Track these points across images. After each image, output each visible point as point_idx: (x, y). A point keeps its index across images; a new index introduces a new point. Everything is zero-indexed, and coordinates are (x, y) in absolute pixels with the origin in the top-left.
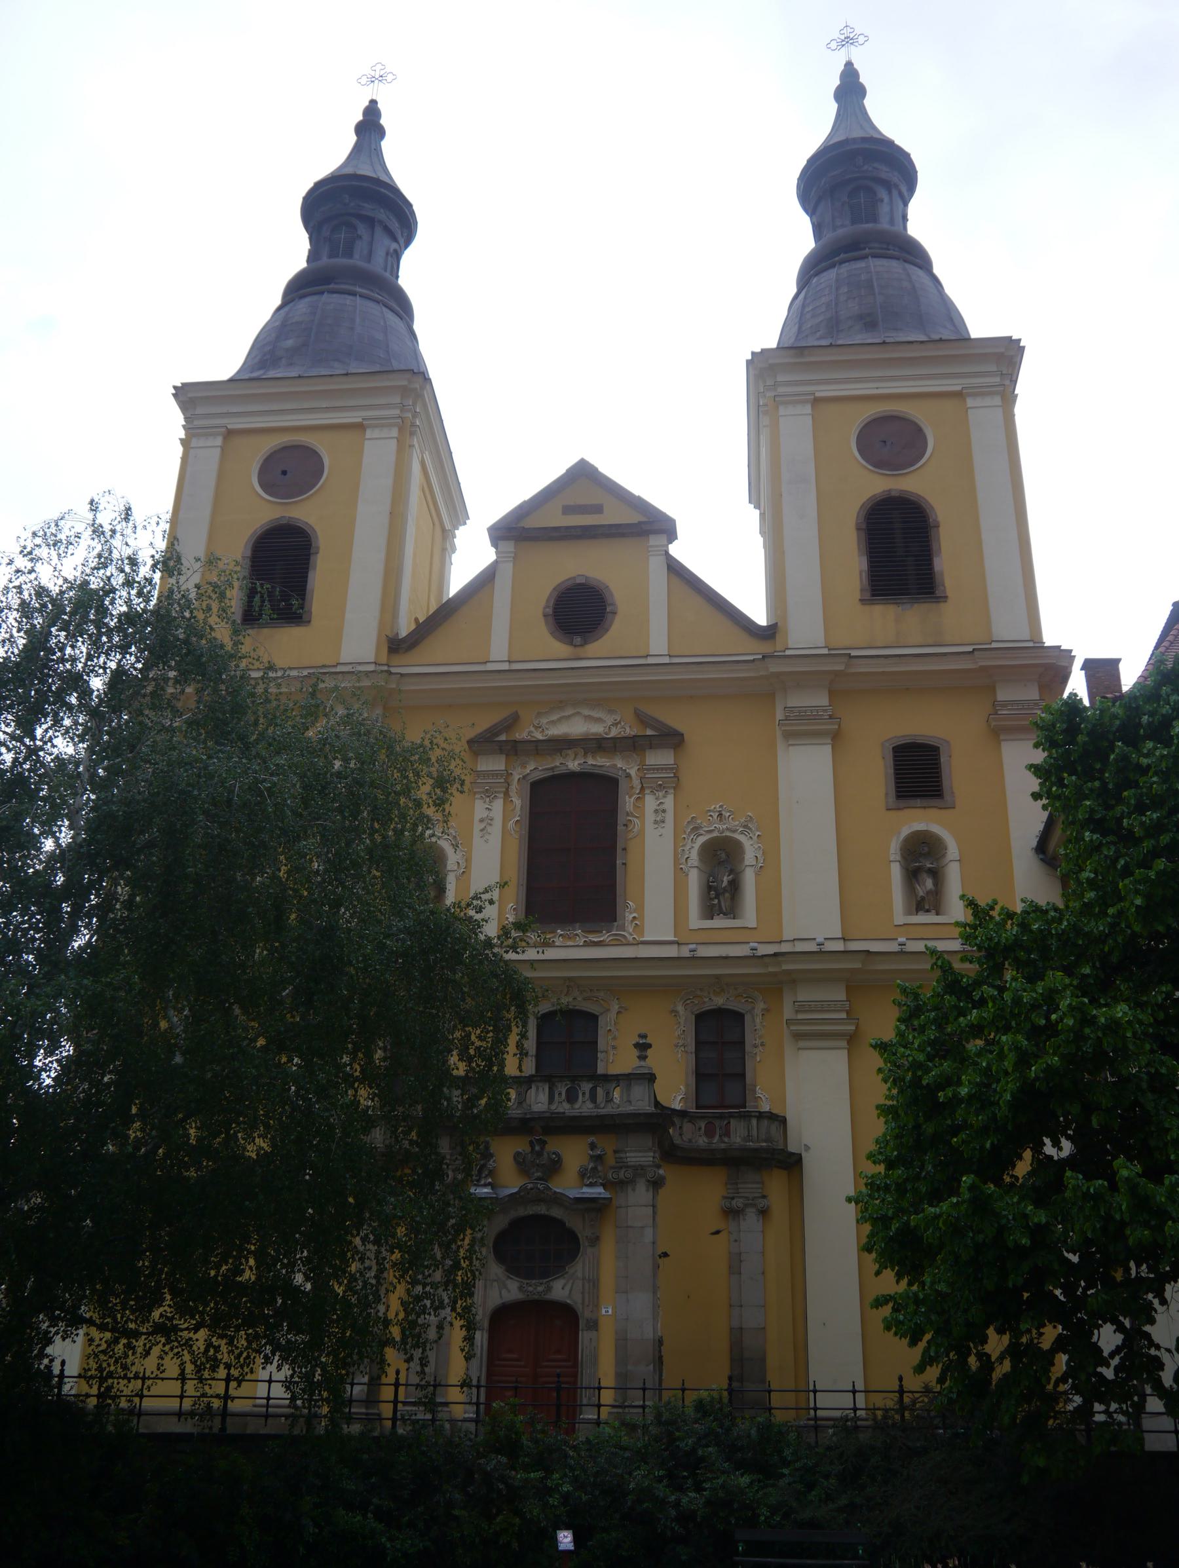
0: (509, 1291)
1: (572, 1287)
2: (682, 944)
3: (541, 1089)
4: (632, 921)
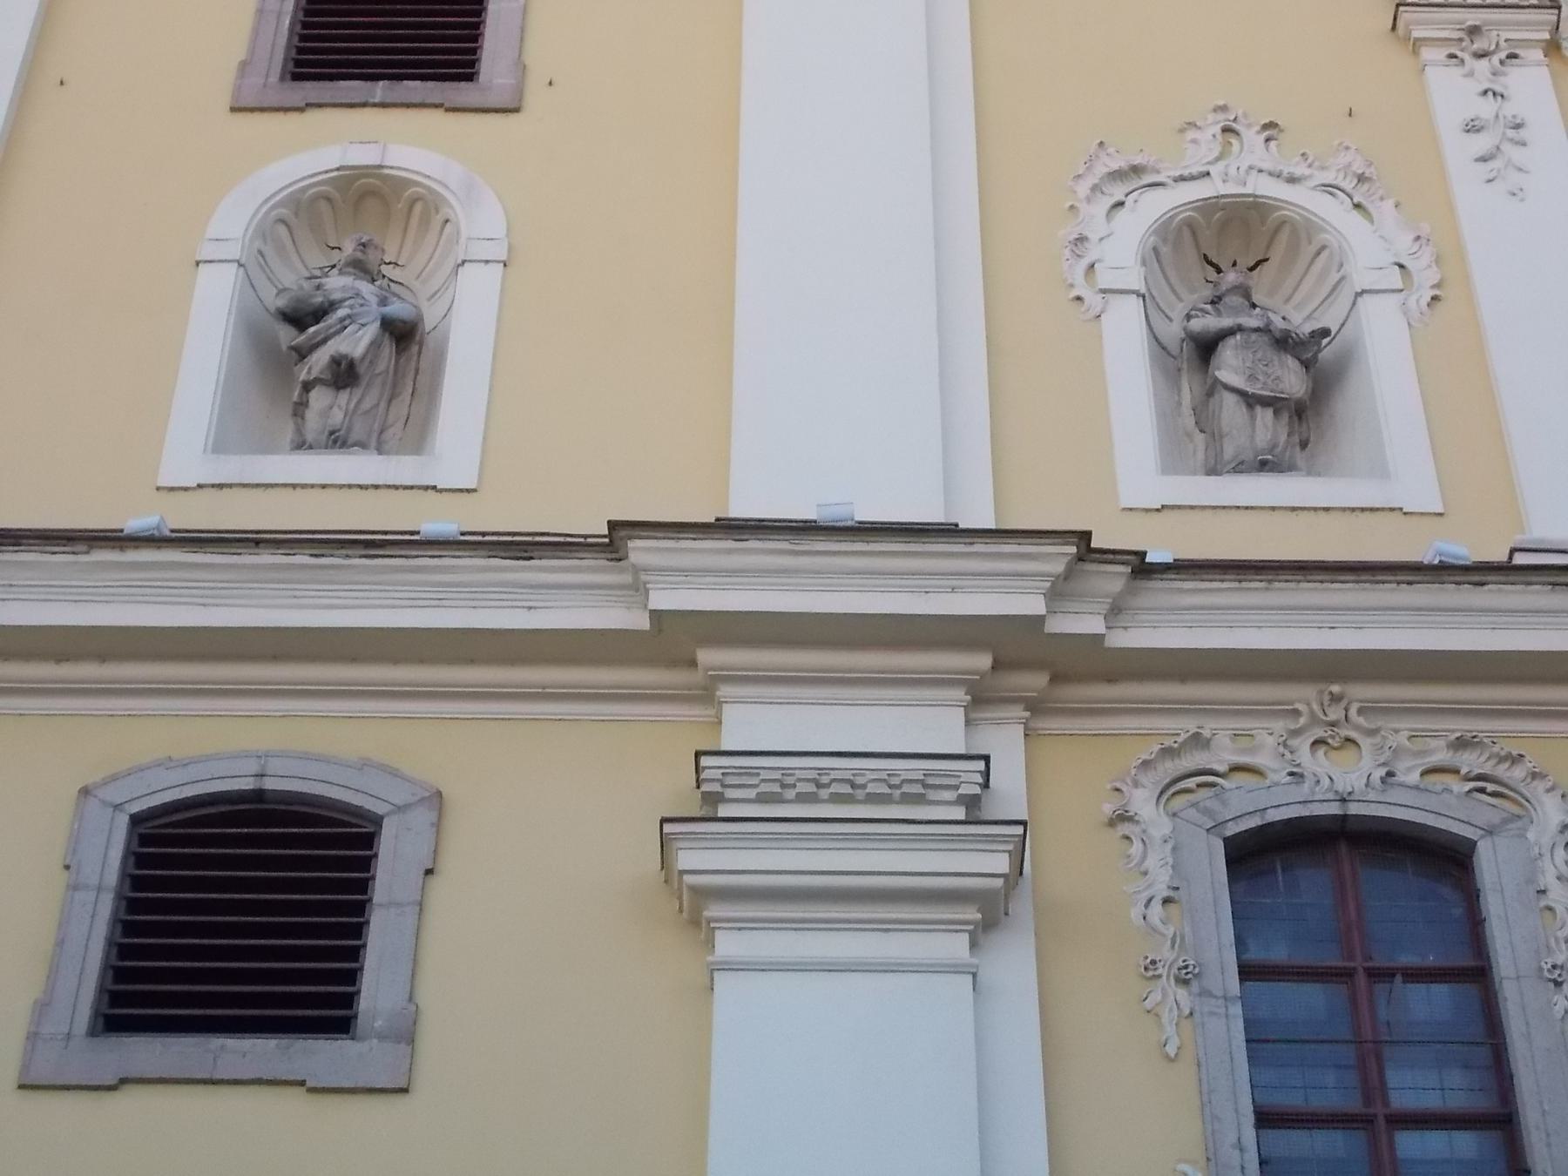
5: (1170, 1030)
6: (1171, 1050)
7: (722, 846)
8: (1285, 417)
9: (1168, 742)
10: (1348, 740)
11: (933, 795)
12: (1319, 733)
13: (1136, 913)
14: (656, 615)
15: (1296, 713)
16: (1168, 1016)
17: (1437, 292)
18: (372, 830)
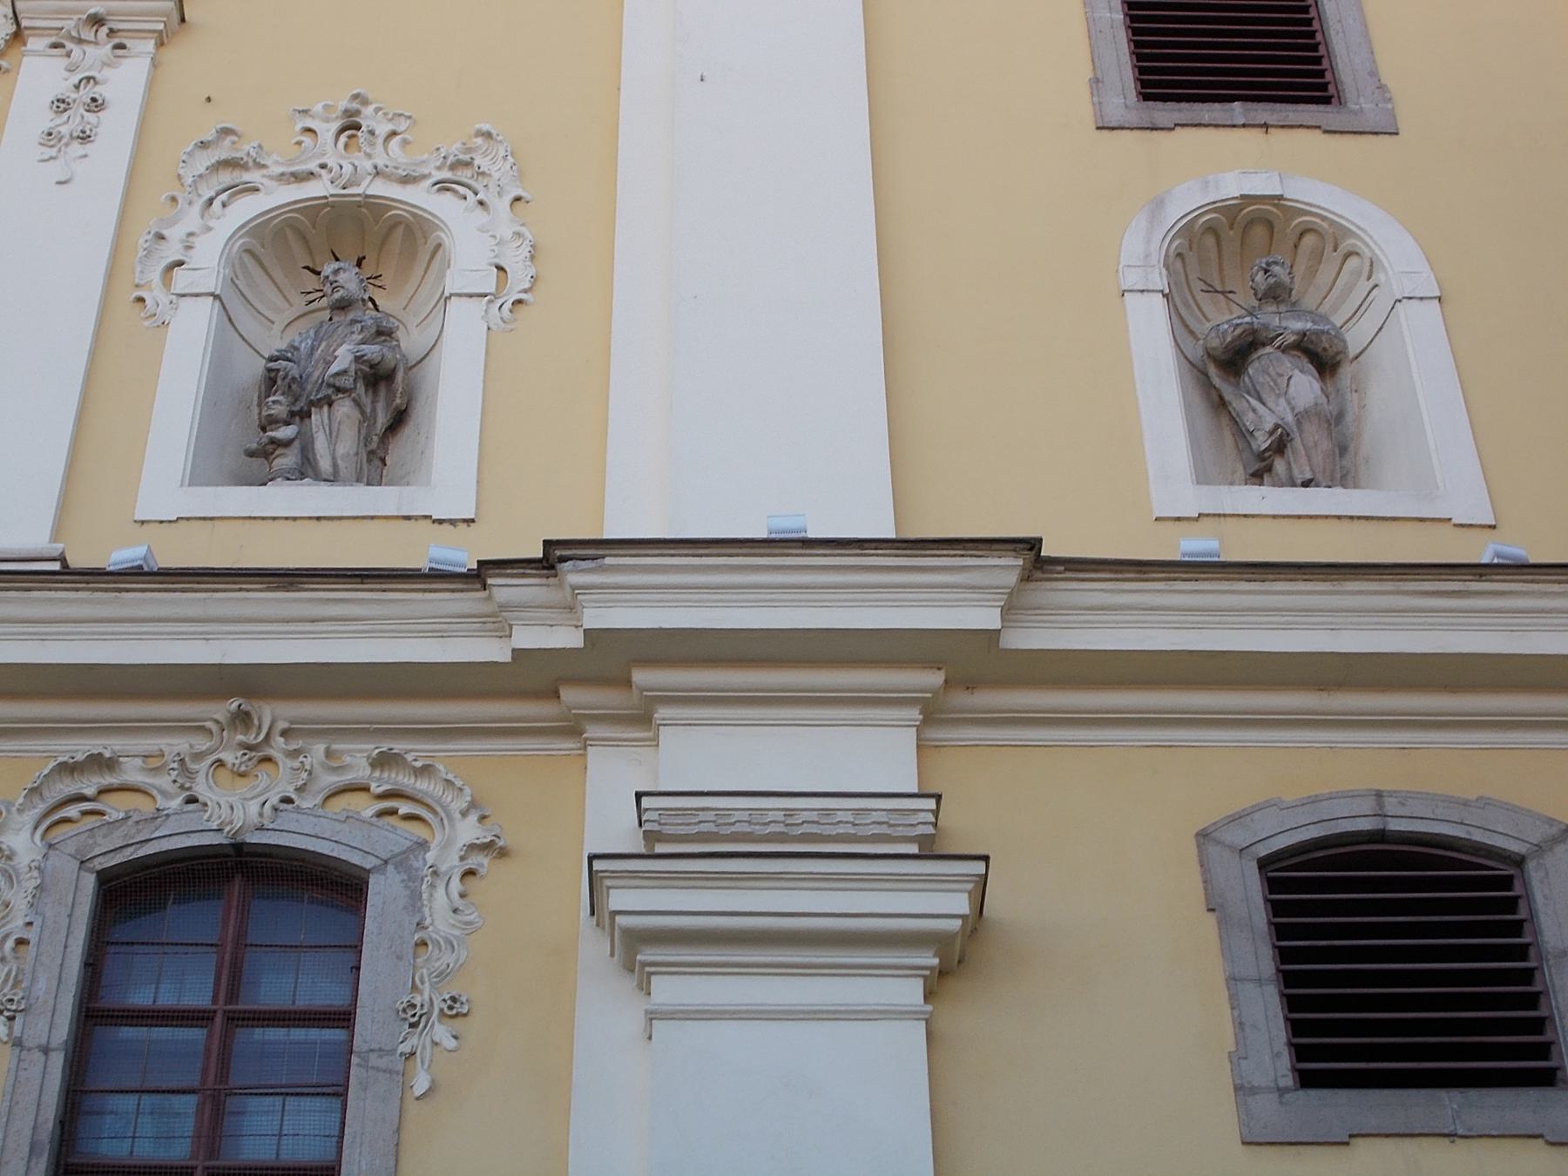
2: (1272, 126)
14: (588, 633)
17: (523, 296)
18: (1511, 872)
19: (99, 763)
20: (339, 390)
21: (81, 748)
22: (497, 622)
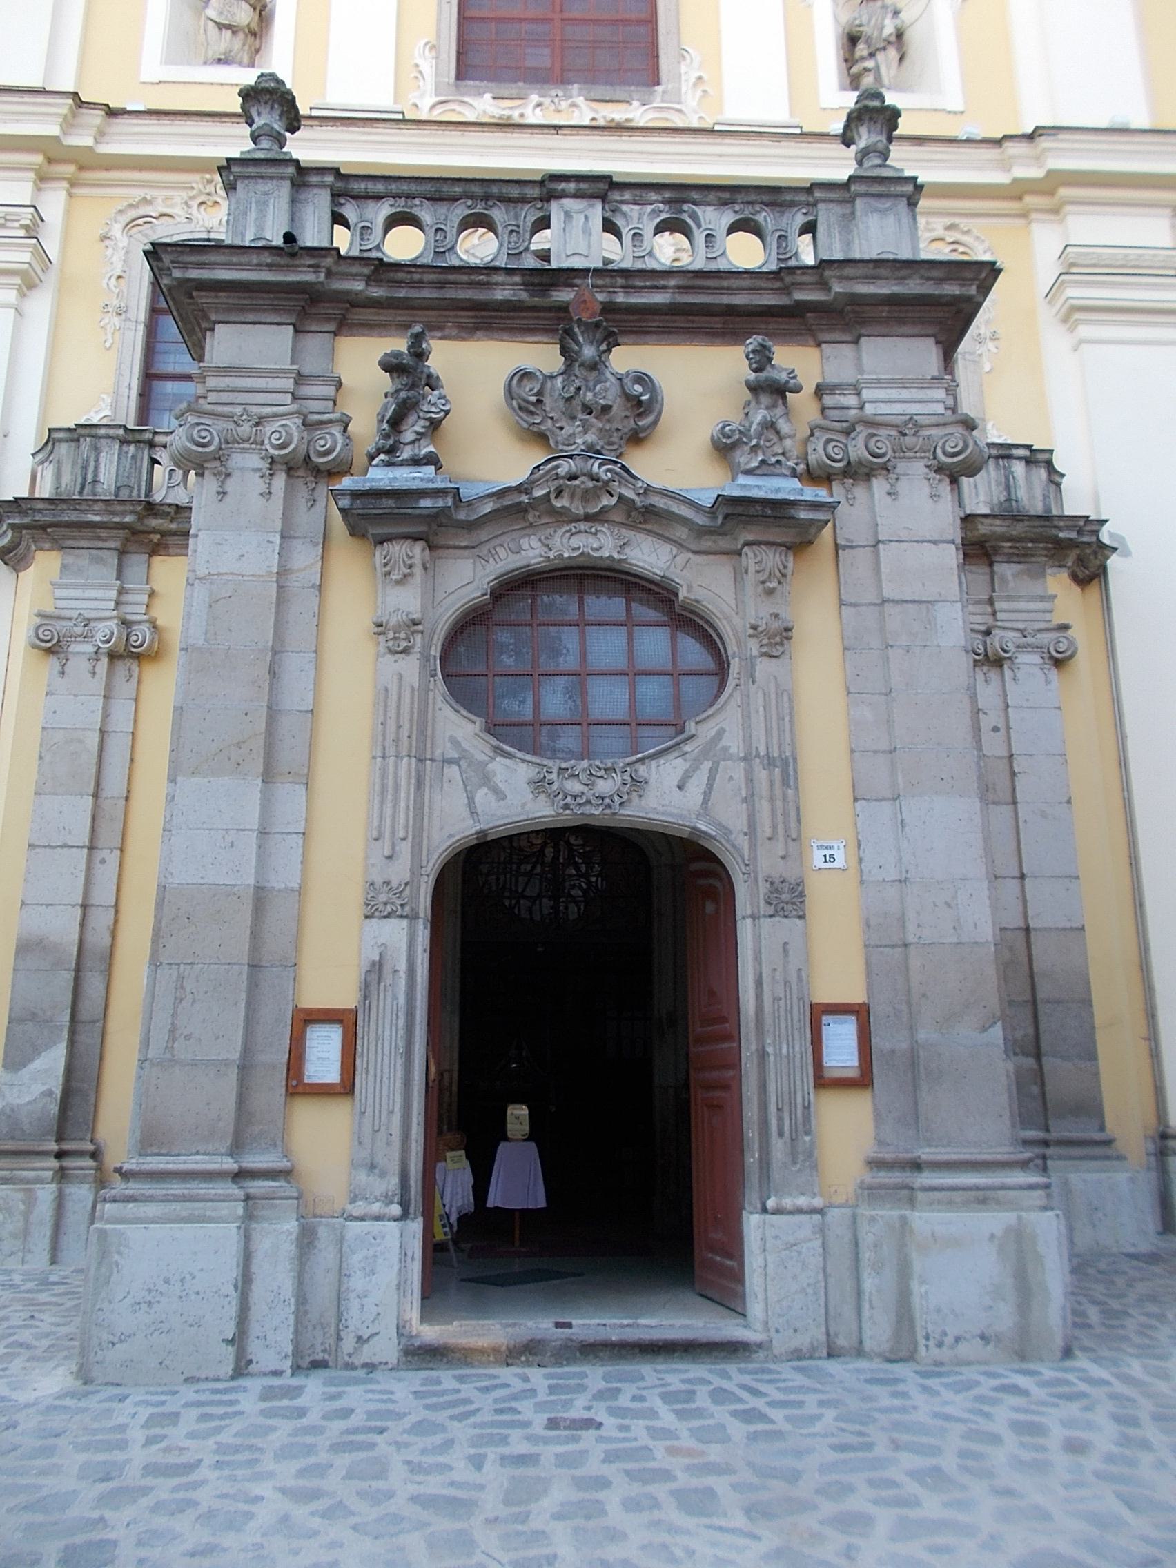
0: (500, 795)
1: (710, 786)
3: (579, 220)
4: (695, 85)
5: (110, 336)
6: (108, 345)
7: (274, 395)
8: (241, 36)
9: (131, 201)
10: (216, 202)
11: (9, 224)
12: (203, 198)
13: (105, 281)
15: (193, 188)
16: (110, 330)
19: (145, 201)
20: (889, 43)
21: (138, 193)
22: (1006, 166)
